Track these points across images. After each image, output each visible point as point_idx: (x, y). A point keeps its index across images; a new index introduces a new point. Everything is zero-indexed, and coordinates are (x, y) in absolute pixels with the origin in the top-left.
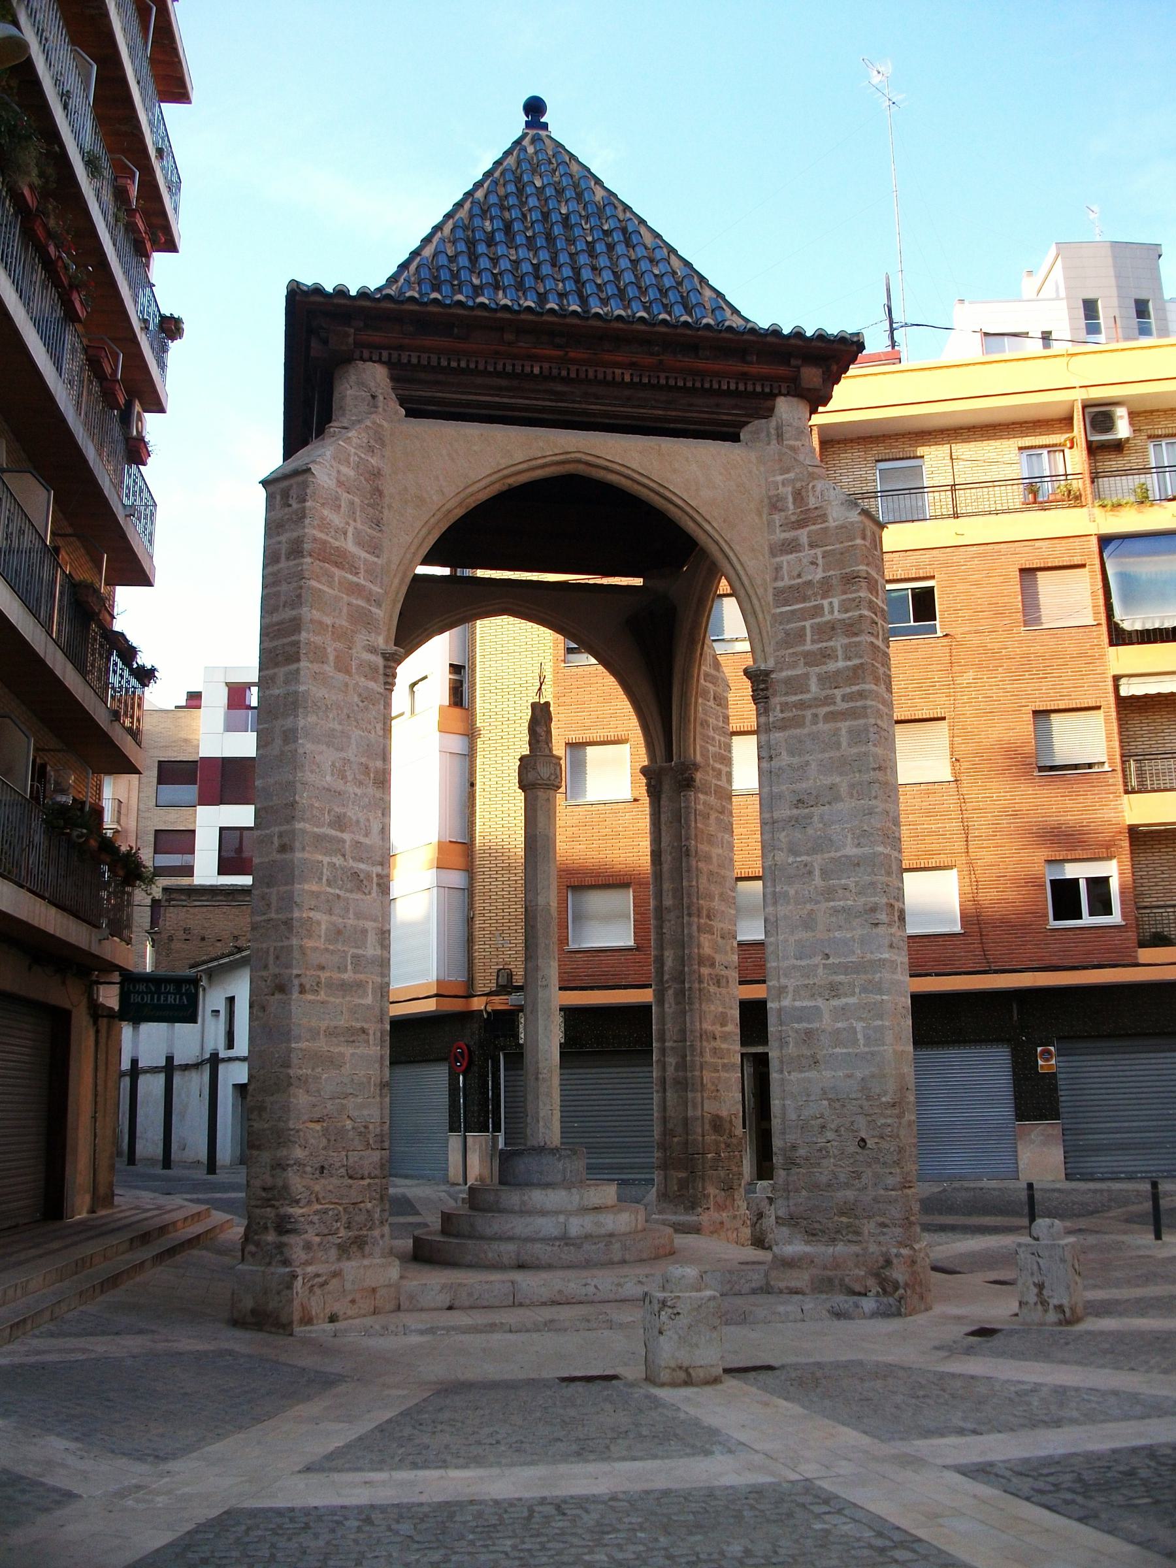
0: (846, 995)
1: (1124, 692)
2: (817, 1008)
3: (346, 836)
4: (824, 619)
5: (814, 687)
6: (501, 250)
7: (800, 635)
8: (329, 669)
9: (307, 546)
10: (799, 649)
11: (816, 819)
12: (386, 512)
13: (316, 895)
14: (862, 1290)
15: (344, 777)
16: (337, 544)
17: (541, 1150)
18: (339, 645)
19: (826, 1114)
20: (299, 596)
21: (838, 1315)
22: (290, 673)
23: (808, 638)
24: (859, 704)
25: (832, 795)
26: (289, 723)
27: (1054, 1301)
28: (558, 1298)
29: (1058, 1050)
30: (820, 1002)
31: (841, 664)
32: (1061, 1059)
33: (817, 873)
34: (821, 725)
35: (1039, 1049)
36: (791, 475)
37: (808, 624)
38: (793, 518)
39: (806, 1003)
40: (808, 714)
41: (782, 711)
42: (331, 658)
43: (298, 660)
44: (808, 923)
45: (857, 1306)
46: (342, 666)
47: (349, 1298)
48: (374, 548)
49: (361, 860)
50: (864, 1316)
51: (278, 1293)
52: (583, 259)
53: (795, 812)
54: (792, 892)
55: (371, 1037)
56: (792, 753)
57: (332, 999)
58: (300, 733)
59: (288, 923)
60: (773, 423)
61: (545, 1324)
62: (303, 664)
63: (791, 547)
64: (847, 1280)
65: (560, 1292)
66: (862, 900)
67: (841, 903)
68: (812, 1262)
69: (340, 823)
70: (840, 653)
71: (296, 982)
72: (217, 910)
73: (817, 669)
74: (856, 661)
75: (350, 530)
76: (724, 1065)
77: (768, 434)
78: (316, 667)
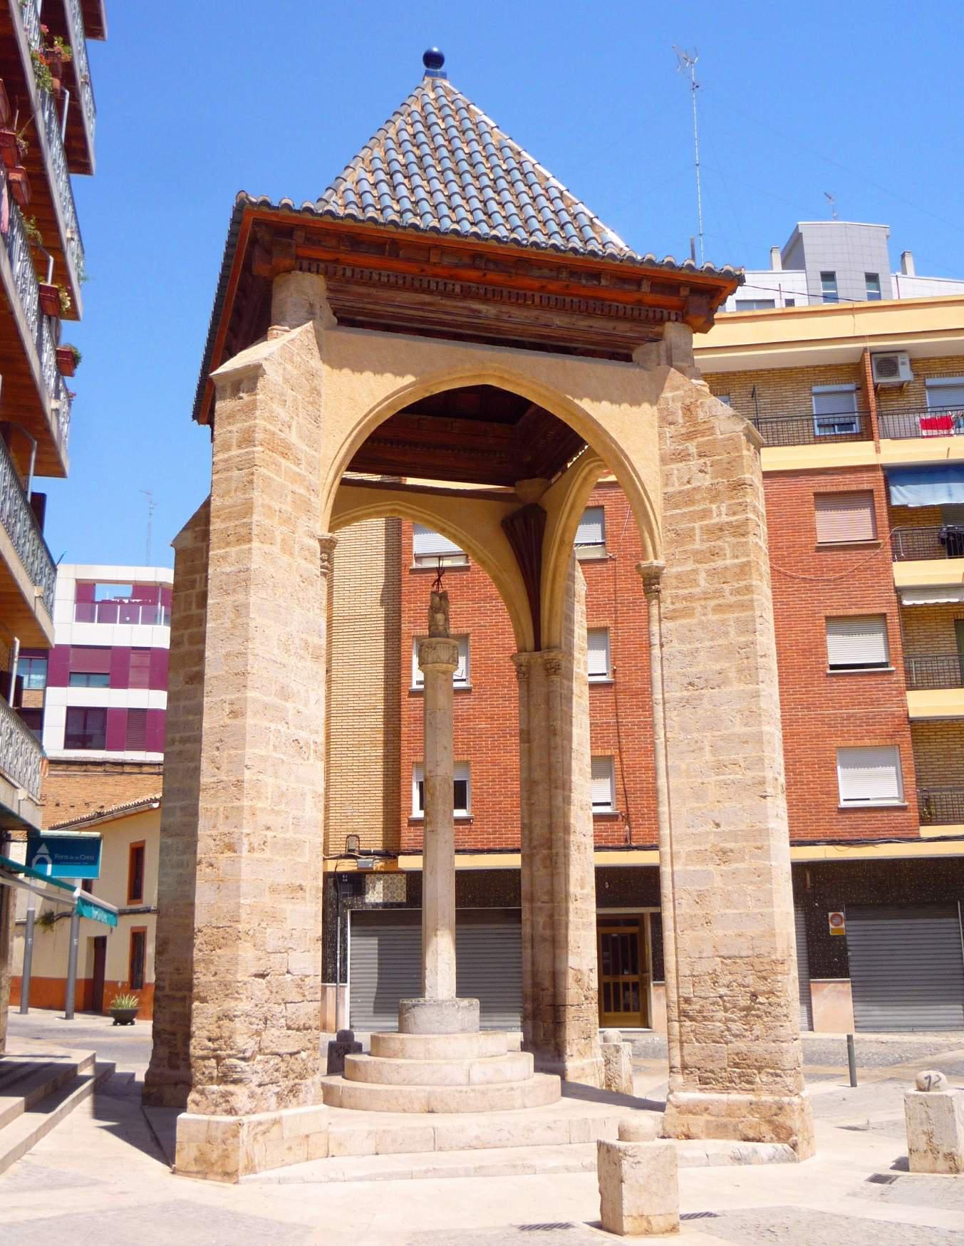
0: (736, 861)
1: (906, 602)
2: (709, 872)
3: (289, 705)
4: (713, 521)
5: (702, 578)
6: (417, 180)
7: (690, 534)
8: (276, 549)
9: (259, 436)
10: (688, 547)
11: (705, 701)
12: (322, 410)
13: (263, 759)
14: (756, 1136)
15: (287, 651)
16: (283, 435)
17: (438, 1004)
18: (284, 529)
19: (719, 970)
20: (251, 482)
21: (738, 1159)
22: (242, 551)
23: (697, 538)
24: (746, 597)
25: (721, 680)
26: (241, 597)
27: (945, 1149)
28: (475, 1143)
29: (846, 915)
30: (711, 867)
31: (729, 562)
32: (851, 923)
33: (708, 748)
34: (710, 616)
35: (830, 914)
36: (681, 392)
37: (697, 525)
38: (683, 431)
39: (698, 867)
40: (697, 605)
41: (673, 603)
42: (279, 540)
43: (250, 541)
44: (698, 794)
45: (755, 1152)
46: (287, 548)
47: (286, 1146)
48: (313, 443)
49: (301, 728)
50: (762, 1162)
51: (224, 1142)
52: (489, 193)
53: (685, 693)
54: (684, 766)
55: (307, 895)
56: (682, 641)
57: (276, 857)
58: (252, 608)
59: (239, 784)
60: (663, 345)
61: (476, 1170)
62: (255, 544)
63: (682, 456)
64: (740, 1126)
65: (477, 1137)
66: (750, 774)
67: (731, 777)
68: (707, 1109)
69: (284, 694)
70: (728, 552)
71: (245, 841)
72: (71, 780)
73: (706, 566)
74: (744, 560)
75: (294, 424)
76: (583, 924)
77: (659, 356)
78: (266, 547)
